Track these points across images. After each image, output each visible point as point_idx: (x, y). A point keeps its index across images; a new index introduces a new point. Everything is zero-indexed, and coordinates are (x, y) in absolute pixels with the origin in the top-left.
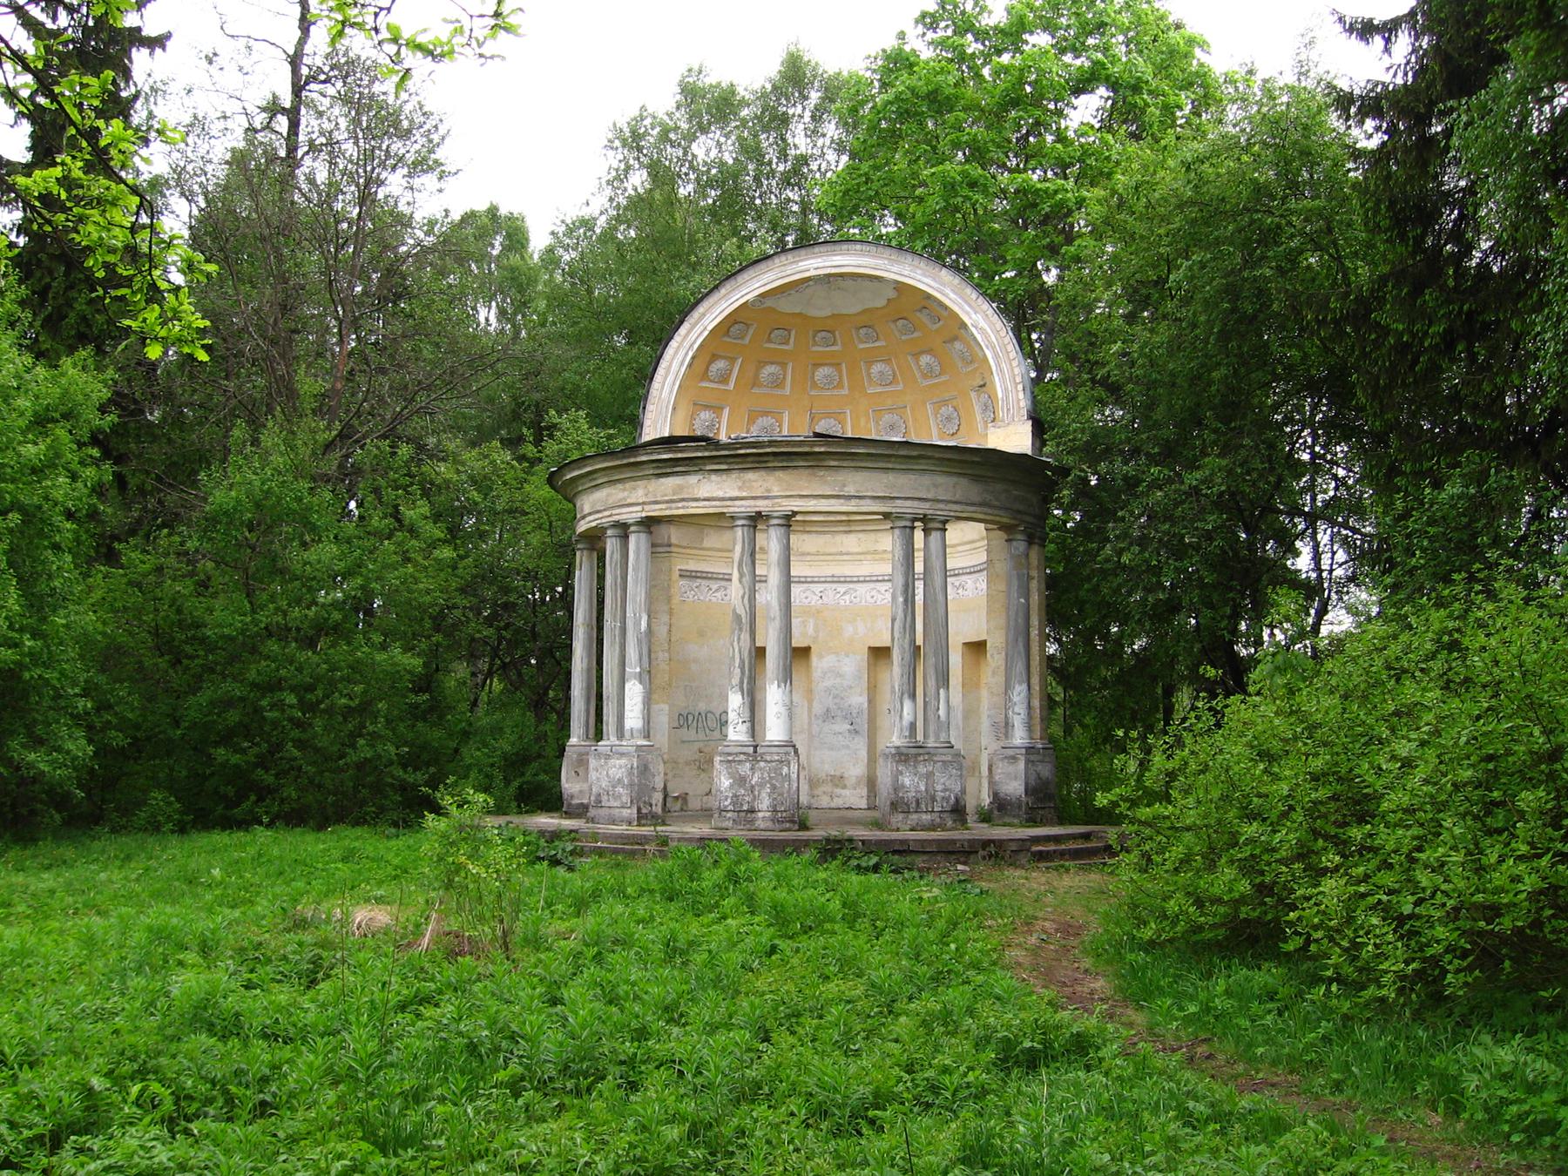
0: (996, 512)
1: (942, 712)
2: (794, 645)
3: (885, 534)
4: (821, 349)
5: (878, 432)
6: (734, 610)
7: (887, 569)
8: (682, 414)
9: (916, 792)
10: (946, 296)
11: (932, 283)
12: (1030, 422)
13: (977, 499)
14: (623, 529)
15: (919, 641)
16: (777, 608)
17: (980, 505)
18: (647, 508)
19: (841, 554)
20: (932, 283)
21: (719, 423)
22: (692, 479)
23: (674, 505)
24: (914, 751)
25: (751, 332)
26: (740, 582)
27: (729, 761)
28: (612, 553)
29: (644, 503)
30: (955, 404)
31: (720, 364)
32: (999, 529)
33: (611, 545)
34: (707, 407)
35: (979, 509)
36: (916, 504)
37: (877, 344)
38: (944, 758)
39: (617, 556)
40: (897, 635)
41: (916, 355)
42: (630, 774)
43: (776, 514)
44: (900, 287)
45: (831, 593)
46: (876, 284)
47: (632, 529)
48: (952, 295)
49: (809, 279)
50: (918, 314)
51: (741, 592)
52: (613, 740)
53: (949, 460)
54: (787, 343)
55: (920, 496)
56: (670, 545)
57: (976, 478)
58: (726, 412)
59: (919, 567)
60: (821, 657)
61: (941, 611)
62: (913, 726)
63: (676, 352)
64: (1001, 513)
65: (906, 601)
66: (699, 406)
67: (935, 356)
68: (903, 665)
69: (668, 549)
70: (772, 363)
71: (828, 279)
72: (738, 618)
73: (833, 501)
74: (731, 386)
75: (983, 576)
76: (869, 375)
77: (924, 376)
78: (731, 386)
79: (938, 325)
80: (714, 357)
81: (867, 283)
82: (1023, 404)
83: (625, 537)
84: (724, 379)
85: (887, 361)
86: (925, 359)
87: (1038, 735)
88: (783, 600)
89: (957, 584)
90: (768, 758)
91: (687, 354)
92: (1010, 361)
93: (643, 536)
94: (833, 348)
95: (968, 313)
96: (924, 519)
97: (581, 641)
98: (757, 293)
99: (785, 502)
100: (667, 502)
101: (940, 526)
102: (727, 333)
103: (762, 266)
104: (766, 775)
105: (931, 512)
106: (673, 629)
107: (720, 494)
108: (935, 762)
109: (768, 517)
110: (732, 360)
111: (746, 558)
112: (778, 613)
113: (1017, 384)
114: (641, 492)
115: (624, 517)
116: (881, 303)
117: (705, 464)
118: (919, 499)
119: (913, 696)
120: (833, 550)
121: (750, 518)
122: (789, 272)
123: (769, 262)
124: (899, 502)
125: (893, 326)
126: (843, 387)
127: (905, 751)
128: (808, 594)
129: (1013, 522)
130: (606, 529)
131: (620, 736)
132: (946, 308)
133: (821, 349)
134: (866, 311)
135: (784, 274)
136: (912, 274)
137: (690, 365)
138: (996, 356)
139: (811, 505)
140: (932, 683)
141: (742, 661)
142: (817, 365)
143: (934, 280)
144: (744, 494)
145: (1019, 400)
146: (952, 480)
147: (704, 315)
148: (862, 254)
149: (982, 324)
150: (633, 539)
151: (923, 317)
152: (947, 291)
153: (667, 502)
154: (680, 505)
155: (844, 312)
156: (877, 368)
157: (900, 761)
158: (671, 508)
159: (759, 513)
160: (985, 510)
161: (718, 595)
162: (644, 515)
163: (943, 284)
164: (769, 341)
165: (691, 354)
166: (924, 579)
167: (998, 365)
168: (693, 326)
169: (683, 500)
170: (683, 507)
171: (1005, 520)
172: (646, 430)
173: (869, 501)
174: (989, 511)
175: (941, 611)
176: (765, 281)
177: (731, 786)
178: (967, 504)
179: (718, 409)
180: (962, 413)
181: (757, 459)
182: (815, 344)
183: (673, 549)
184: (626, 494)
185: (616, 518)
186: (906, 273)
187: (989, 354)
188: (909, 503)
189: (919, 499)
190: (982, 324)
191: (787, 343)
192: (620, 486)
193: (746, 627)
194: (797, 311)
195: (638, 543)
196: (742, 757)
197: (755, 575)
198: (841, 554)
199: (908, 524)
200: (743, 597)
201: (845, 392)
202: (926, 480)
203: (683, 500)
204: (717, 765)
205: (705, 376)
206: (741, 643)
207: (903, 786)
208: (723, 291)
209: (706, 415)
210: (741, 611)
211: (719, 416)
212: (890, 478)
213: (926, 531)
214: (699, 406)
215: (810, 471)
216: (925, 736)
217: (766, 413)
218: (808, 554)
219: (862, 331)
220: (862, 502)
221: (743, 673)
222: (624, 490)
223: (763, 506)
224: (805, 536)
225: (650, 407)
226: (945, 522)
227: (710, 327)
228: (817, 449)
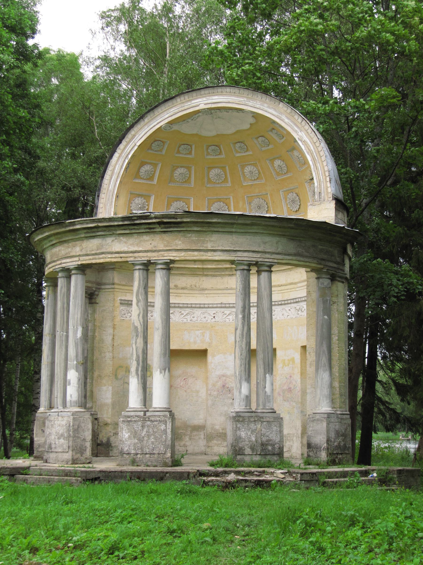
0: (306, 260)
1: (268, 389)
2: (173, 347)
3: (326, 280)
4: (212, 157)
5: (251, 210)
6: (134, 323)
7: (232, 299)
8: (123, 200)
9: (250, 441)
10: (283, 120)
11: (274, 113)
12: (334, 202)
13: (293, 251)
14: (67, 272)
15: (254, 345)
16: (160, 322)
17: (295, 255)
18: (81, 258)
19: (227, 289)
20: (274, 113)
21: (148, 205)
22: (109, 240)
23: (97, 257)
24: (249, 414)
25: (166, 146)
26: (137, 305)
27: (129, 421)
28: (62, 288)
29: (79, 256)
30: (297, 191)
31: (147, 168)
32: (312, 271)
33: (61, 282)
34: (139, 196)
35: (294, 258)
36: (251, 254)
37: (247, 153)
38: (268, 419)
39: (65, 290)
40: (238, 339)
41: (272, 161)
42: (69, 431)
43: (160, 262)
44: (255, 115)
45: (220, 315)
46: (241, 114)
47: (73, 272)
48: (286, 120)
49: (198, 112)
50: (270, 133)
51: (138, 313)
52: (61, 408)
53: (273, 226)
54: (220, 154)
55: (253, 250)
56: (113, 284)
57: (292, 238)
58: (153, 198)
59: (254, 298)
60: (213, 356)
61: (268, 323)
62: (248, 398)
63: (118, 160)
64: (310, 260)
65: (244, 317)
66: (133, 195)
67: (283, 161)
68: (241, 359)
69: (113, 286)
70: (181, 167)
71: (210, 111)
72: (136, 328)
73: (196, 253)
74: (155, 182)
75: (304, 305)
76: (243, 173)
77: (278, 174)
78: (155, 182)
79: (283, 140)
80: (143, 164)
81: (235, 113)
82: (329, 190)
83: (69, 277)
84: (151, 178)
85: (254, 165)
86: (277, 163)
87: (338, 405)
88: (164, 317)
89: (298, 308)
90: (153, 419)
91: (124, 161)
92: (322, 162)
93: (80, 277)
94: (220, 157)
95: (296, 132)
96: (257, 264)
97: (48, 345)
98: (166, 121)
99: (166, 254)
100: (93, 255)
101: (246, 267)
102: (150, 148)
103: (170, 103)
104: (151, 430)
105: (261, 260)
106: (116, 338)
107: (126, 249)
108: (262, 422)
109: (155, 264)
110: (155, 165)
111: (142, 290)
112: (160, 326)
113: (326, 177)
114: (78, 249)
115: (68, 264)
116: (246, 126)
117: (116, 230)
118: (254, 252)
119: (248, 379)
120: (222, 287)
121: (144, 264)
122: (186, 107)
123: (174, 101)
124: (239, 254)
125: (255, 141)
126: (228, 182)
127: (242, 414)
128: (206, 315)
129: (319, 266)
130: (57, 272)
131: (64, 405)
132: (282, 127)
133: (212, 157)
134: (237, 132)
135: (183, 109)
136: (262, 107)
137: (126, 168)
138: (313, 159)
139: (182, 255)
140: (261, 370)
141: (138, 356)
142: (210, 168)
143: (275, 110)
144: (141, 249)
145: (327, 188)
146: (275, 239)
147: (134, 136)
148: (230, 94)
149: (305, 138)
150: (73, 278)
151: (273, 135)
152: (283, 117)
153: (93, 255)
154: (101, 256)
155: (225, 133)
156: (247, 169)
157: (238, 421)
158: (95, 259)
159: (149, 261)
160: (299, 258)
161: (188, 317)
162: (79, 263)
163: (281, 113)
164: (178, 152)
165: (127, 161)
166: (257, 306)
167: (315, 164)
168: (128, 143)
169: (103, 253)
170: (102, 258)
171: (313, 265)
172: (100, 210)
173: (219, 253)
174: (302, 259)
175: (268, 323)
176: (172, 113)
177: (130, 437)
178: (285, 255)
179: (147, 197)
180: (301, 197)
181: (148, 226)
182: (208, 154)
183: (116, 286)
184: (70, 250)
185: (63, 265)
186: (258, 106)
187: (309, 158)
188: (246, 254)
189: (254, 252)
190: (305, 138)
191: (190, 153)
192: (66, 245)
193: (141, 334)
194: (195, 132)
195: (76, 281)
196: (136, 419)
197: (147, 302)
198: (227, 289)
199: (246, 267)
200: (139, 315)
201: (229, 184)
202: (258, 239)
203: (103, 253)
204: (121, 424)
205: (137, 175)
206: (138, 345)
207: (240, 438)
208: (146, 120)
209: (139, 201)
210: (137, 324)
211: (148, 201)
212: (234, 238)
213: (259, 272)
214: (133, 195)
215: (181, 234)
216: (258, 405)
217: (219, 200)
218: (206, 289)
219: (238, 145)
220: (216, 254)
221: (138, 364)
222: (68, 247)
223: (153, 257)
224: (204, 278)
225: (102, 196)
226: (270, 266)
227: (138, 144)
228: (185, 220)
